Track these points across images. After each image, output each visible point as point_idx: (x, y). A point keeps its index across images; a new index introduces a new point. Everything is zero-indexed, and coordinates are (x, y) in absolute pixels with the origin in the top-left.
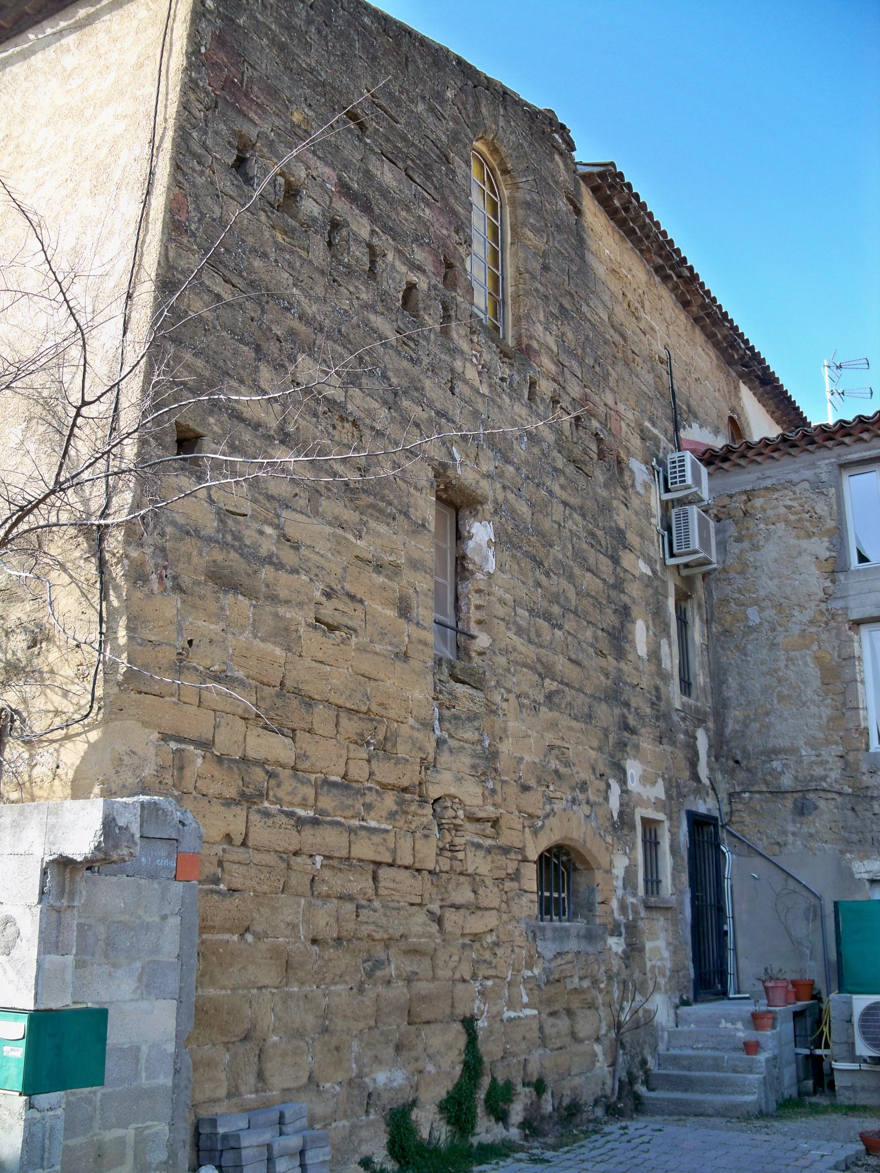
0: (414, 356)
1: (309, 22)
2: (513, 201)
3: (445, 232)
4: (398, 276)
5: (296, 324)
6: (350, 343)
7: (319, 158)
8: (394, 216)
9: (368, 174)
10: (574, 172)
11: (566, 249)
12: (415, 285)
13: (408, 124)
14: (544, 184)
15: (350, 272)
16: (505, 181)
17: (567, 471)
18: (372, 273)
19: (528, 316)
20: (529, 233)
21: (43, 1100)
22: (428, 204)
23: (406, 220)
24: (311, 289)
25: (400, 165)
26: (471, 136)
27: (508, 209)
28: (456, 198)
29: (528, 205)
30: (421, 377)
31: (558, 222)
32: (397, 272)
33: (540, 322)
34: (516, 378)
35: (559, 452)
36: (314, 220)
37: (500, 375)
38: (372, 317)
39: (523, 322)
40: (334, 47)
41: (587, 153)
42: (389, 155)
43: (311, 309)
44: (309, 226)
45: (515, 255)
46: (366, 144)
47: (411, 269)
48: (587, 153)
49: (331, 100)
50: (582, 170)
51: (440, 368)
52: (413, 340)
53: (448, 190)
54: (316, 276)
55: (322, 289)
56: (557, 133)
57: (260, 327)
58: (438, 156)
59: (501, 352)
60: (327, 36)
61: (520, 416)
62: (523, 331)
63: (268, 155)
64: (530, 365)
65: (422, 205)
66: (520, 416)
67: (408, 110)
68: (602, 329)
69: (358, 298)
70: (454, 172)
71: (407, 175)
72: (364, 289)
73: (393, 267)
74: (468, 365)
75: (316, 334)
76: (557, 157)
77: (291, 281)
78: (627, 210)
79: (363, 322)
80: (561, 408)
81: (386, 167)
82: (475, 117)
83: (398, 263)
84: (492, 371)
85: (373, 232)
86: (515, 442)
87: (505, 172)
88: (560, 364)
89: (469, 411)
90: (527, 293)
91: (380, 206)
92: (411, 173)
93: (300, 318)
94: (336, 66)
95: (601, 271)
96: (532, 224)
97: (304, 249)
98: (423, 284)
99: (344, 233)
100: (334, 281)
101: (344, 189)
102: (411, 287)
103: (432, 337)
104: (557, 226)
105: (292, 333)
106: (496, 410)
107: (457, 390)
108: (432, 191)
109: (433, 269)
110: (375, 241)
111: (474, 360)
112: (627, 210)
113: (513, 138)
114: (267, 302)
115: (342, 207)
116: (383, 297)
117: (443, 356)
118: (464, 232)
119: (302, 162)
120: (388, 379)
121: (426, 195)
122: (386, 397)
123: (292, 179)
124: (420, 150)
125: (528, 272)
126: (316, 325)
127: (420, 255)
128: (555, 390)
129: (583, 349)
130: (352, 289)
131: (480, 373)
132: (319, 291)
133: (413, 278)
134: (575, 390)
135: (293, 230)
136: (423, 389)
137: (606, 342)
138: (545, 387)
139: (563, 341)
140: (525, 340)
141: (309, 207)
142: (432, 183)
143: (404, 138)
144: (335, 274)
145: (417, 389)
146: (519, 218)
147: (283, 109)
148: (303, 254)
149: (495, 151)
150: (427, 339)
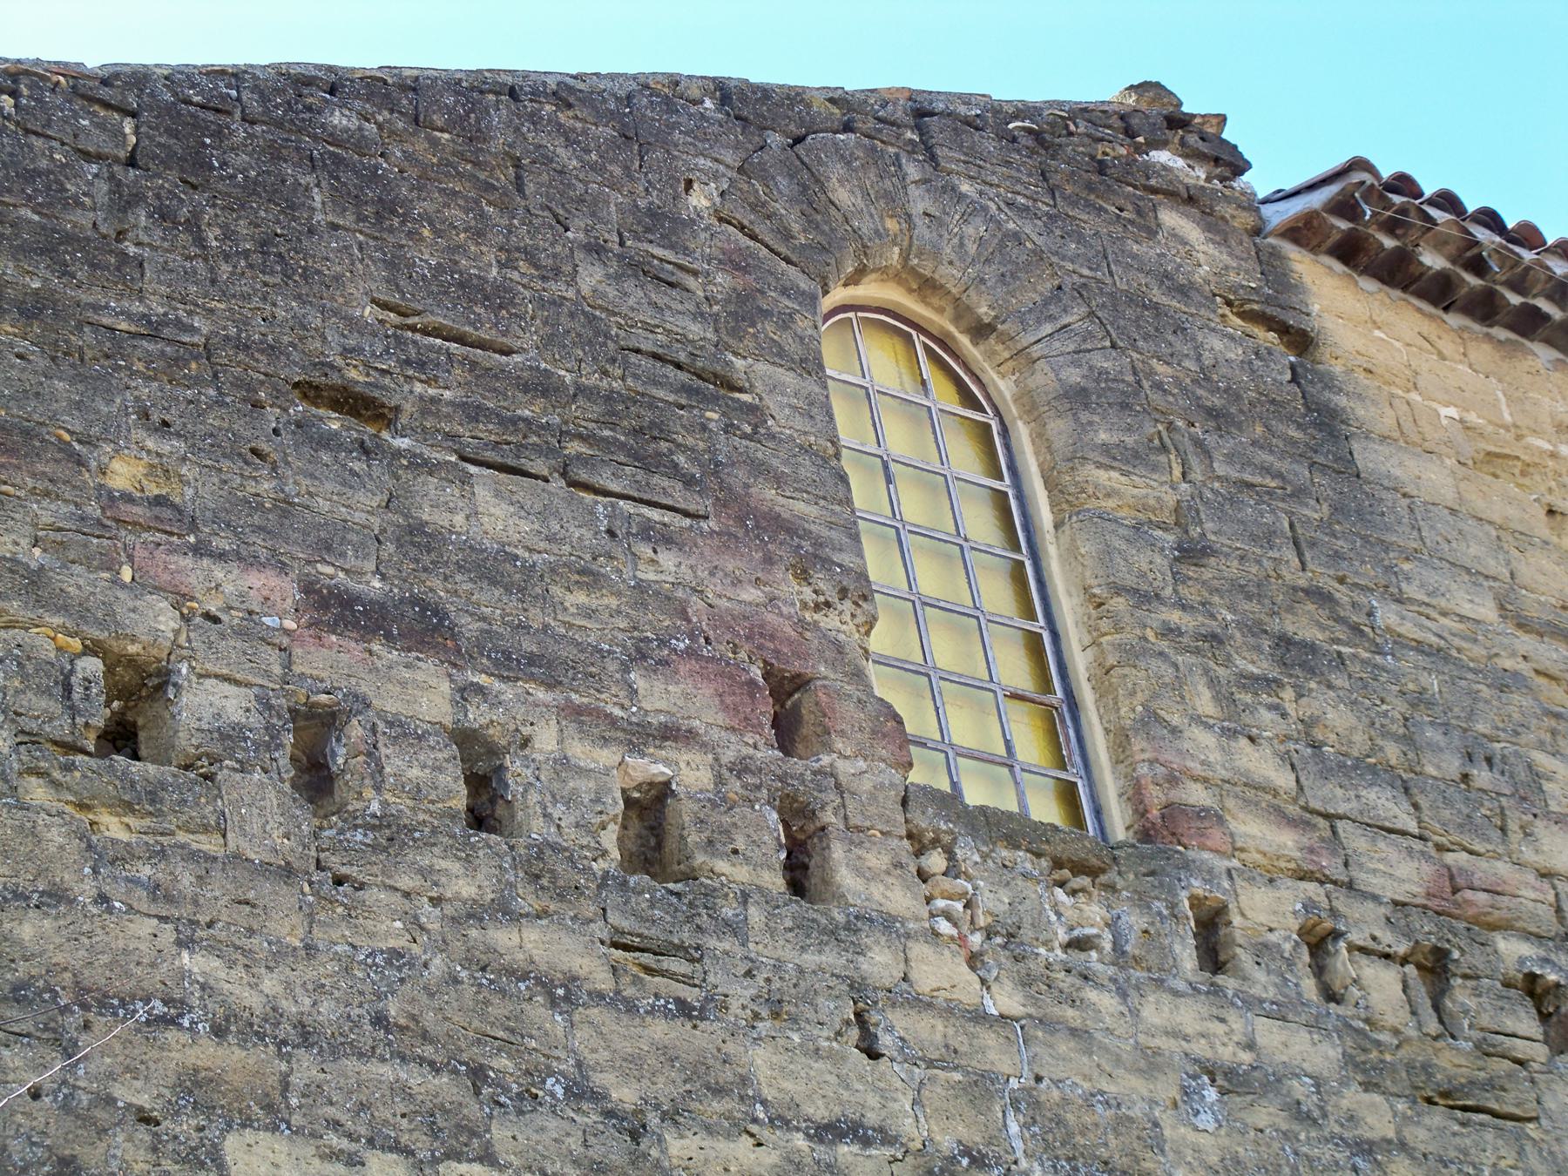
0: (692, 995)
1: (124, 201)
2: (1030, 405)
3: (751, 594)
4: (585, 787)
5: (207, 1054)
6: (425, 1036)
7: (221, 556)
8: (536, 617)
9: (419, 539)
10: (1257, 232)
11: (1266, 470)
12: (667, 784)
13: (548, 342)
14: (1141, 314)
15: (392, 835)
16: (990, 355)
17: (1418, 1136)
18: (486, 807)
19: (1151, 719)
20: (1103, 476)
21: (143, 752)
22: (667, 539)
23: (590, 613)
24: (251, 932)
25: (539, 466)
26: (804, 284)
27: (1023, 433)
28: (779, 481)
29: (1077, 398)
30: (730, 1048)
31: (1217, 401)
32: (573, 774)
33: (1198, 720)
34: (1134, 921)
35: (1368, 1086)
36: (230, 736)
37: (1063, 936)
38: (503, 938)
39: (1138, 743)
40: (228, 234)
41: (1283, 159)
42: (489, 455)
43: (251, 993)
44: (214, 760)
45: (1071, 555)
46: (398, 454)
47: (635, 748)
48: (1283, 159)
49: (238, 384)
50: (1277, 215)
51: (809, 998)
52: (680, 950)
53: (741, 473)
54: (263, 891)
55: (296, 919)
56: (1161, 145)
57: (66, 1108)
58: (686, 389)
59: (1058, 864)
60: (196, 215)
61: (1175, 1034)
62: (1143, 769)
63: (26, 615)
64: (1187, 865)
65: (645, 550)
66: (1175, 1034)
67: (541, 303)
68: (1478, 651)
69: (436, 901)
70: (754, 412)
71: (573, 484)
72: (455, 867)
73: (563, 764)
74: (918, 949)
75: (288, 1058)
76: (1170, 218)
77: (168, 934)
78: (1478, 266)
79: (467, 962)
80: (1352, 948)
81: (483, 493)
82: (811, 225)
83: (580, 751)
84: (1027, 934)
85: (465, 692)
86: (1166, 1118)
87: (981, 331)
88: (1306, 817)
89: (951, 1086)
90: (1133, 654)
91: (477, 608)
92: (583, 475)
93: (219, 1032)
94: (243, 286)
95: (1435, 479)
96: (1106, 448)
97: (206, 829)
98: (690, 773)
99: (356, 731)
100: (339, 881)
101: (335, 610)
102: (650, 809)
103: (755, 915)
104: (1212, 413)
105: (195, 1088)
106: (1064, 1046)
107: (886, 1042)
108: (678, 495)
109: (721, 718)
110: (477, 715)
111: (944, 927)
112: (1478, 266)
113: (976, 228)
114: (87, 1026)
115: (331, 663)
116: (537, 866)
117: (810, 959)
118: (827, 563)
119: (157, 589)
120: (597, 1096)
121: (655, 514)
122: (596, 1153)
123: (132, 649)
124: (609, 398)
125: (1118, 590)
126: (286, 1030)
127: (657, 696)
128: (1310, 905)
129: (1408, 740)
130: (406, 882)
131: (974, 960)
132: (288, 928)
133: (650, 767)
134: (1399, 873)
135: (153, 795)
136: (744, 1081)
137: (1505, 683)
138: (1266, 912)
139: (1316, 746)
140: (1156, 797)
141: (206, 702)
142: (675, 471)
143: (543, 386)
144: (334, 861)
145: (719, 1091)
146: (1059, 443)
147: (63, 471)
148: (208, 844)
149: (927, 287)
150: (735, 929)
